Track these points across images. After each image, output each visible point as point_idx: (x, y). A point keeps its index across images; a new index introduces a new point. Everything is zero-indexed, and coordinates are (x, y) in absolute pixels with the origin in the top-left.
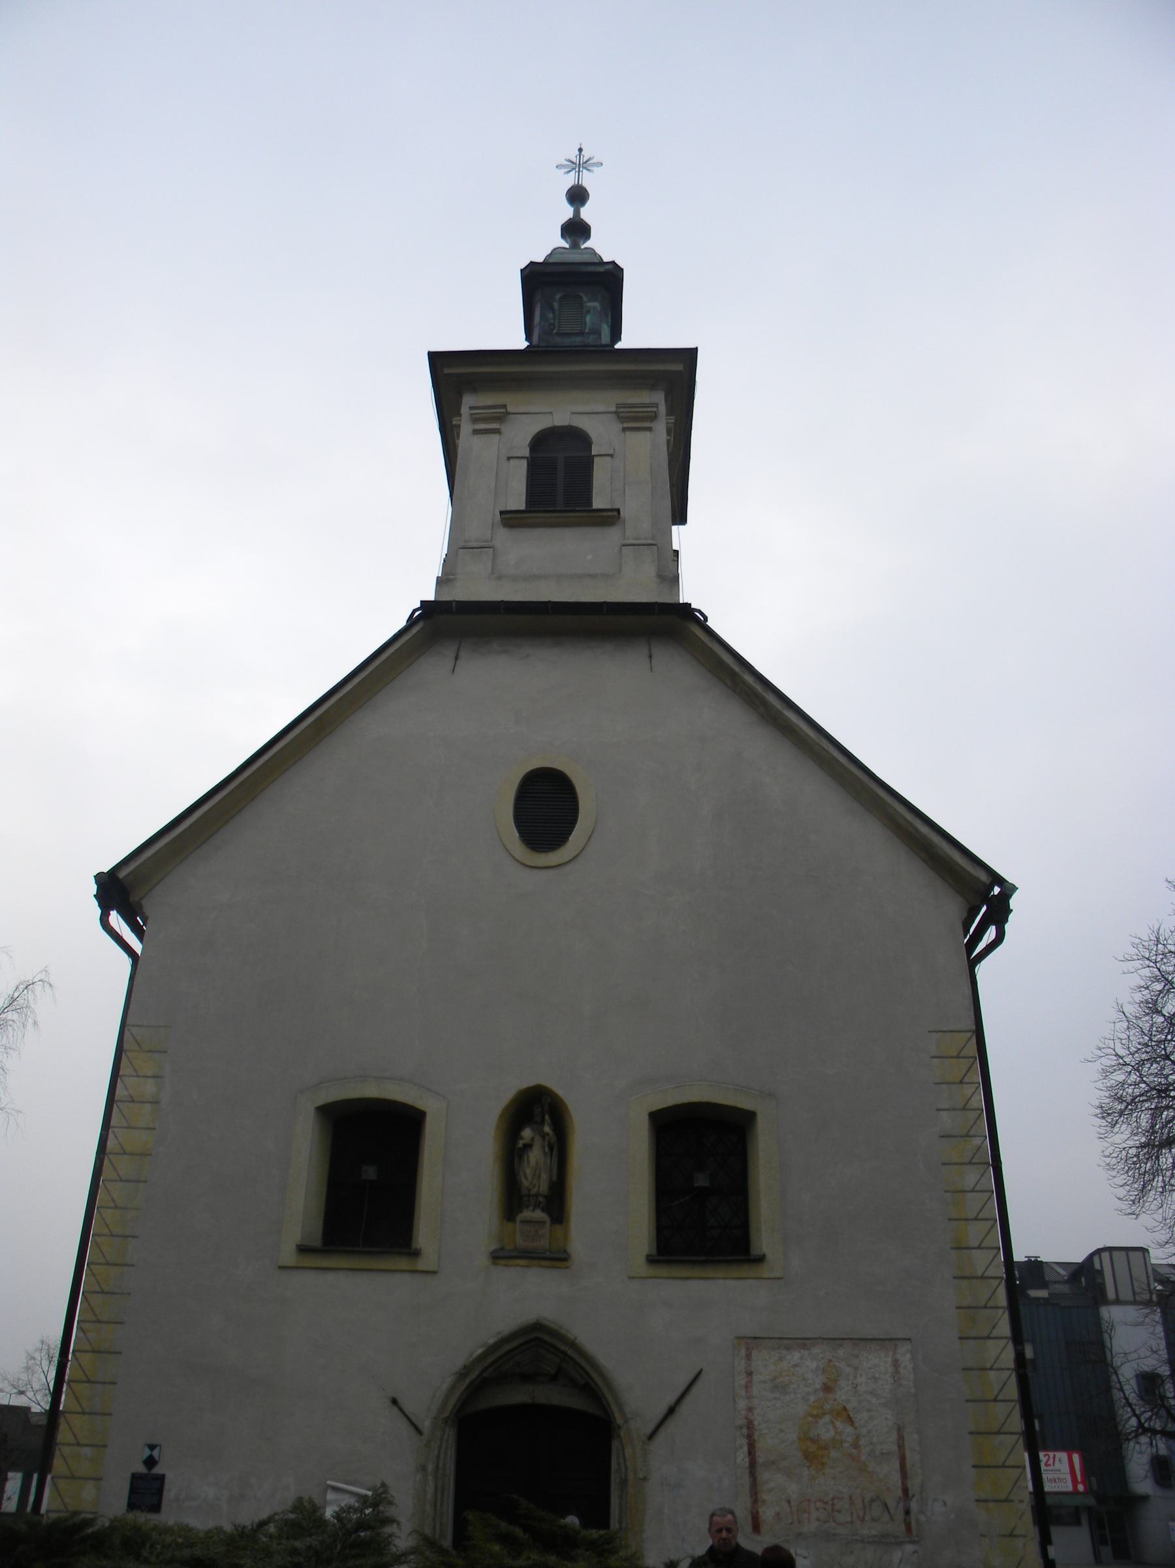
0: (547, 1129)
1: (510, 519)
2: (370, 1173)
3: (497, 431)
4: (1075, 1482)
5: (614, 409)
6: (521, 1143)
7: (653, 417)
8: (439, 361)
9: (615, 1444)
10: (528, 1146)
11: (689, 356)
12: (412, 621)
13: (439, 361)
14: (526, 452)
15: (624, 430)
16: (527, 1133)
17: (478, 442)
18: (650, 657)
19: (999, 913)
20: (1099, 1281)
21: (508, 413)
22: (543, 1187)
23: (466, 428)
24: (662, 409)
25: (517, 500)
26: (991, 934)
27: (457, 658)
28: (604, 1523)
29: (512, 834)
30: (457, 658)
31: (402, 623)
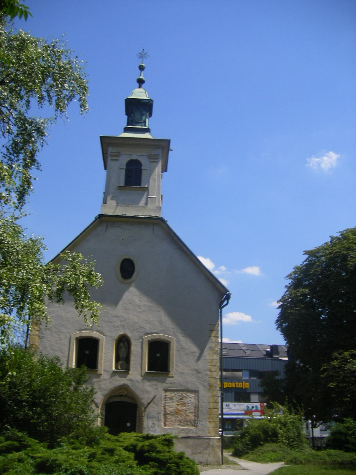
0: (126, 343)
1: (120, 188)
2: (87, 352)
3: (117, 160)
4: (228, 414)
5: (148, 155)
6: (120, 347)
7: (157, 158)
8: (102, 138)
9: (138, 409)
10: (121, 347)
11: (168, 141)
12: (96, 219)
13: (102, 138)
14: (125, 167)
15: (151, 162)
16: (121, 344)
17: (113, 163)
18: (153, 229)
19: (228, 297)
20: (82, 473)
21: (121, 154)
22: (125, 356)
23: (109, 158)
24: (161, 155)
25: (122, 184)
26: (225, 302)
27: (107, 227)
28: (56, 103)
29: (119, 275)
30: (107, 227)
31: (94, 219)
